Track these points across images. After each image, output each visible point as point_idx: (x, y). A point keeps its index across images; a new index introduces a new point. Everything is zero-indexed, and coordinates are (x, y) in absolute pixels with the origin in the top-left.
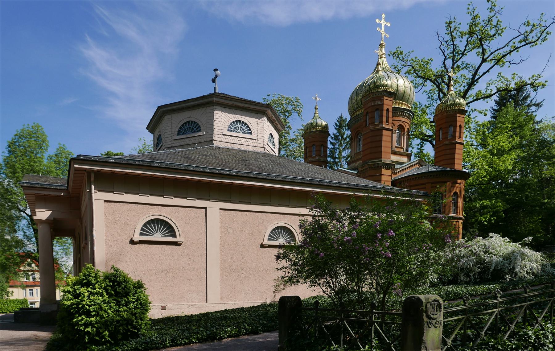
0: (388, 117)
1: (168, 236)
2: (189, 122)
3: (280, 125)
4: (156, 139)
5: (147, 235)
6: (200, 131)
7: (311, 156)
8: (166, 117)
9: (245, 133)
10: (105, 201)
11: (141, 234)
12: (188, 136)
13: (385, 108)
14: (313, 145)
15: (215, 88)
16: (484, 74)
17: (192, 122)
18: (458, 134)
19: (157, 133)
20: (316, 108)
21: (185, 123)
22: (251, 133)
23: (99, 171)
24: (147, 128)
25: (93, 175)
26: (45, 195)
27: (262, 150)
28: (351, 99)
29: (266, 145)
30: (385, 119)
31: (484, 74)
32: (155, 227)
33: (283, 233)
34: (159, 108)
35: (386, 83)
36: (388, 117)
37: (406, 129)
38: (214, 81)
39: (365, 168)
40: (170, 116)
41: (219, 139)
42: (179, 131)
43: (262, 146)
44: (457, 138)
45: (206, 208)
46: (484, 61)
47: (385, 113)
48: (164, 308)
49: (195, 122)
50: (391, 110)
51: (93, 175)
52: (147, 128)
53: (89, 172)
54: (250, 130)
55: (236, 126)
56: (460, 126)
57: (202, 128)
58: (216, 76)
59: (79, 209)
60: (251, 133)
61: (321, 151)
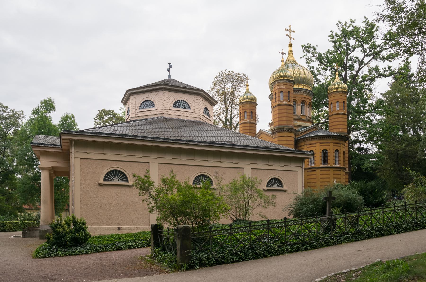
2: (147, 100)
5: (109, 180)
7: (244, 119)
9: (185, 108)
10: (81, 158)
11: (105, 180)
14: (245, 111)
17: (149, 100)
21: (145, 101)
22: (190, 108)
23: (78, 140)
24: (122, 102)
25: (73, 143)
27: (197, 120)
32: (114, 175)
34: (128, 91)
35: (286, 74)
38: (168, 70)
43: (198, 117)
45: (149, 163)
48: (119, 229)
49: (151, 101)
51: (73, 143)
52: (122, 102)
53: (71, 141)
54: (189, 106)
55: (178, 104)
57: (155, 105)
59: (69, 160)
60: (190, 108)
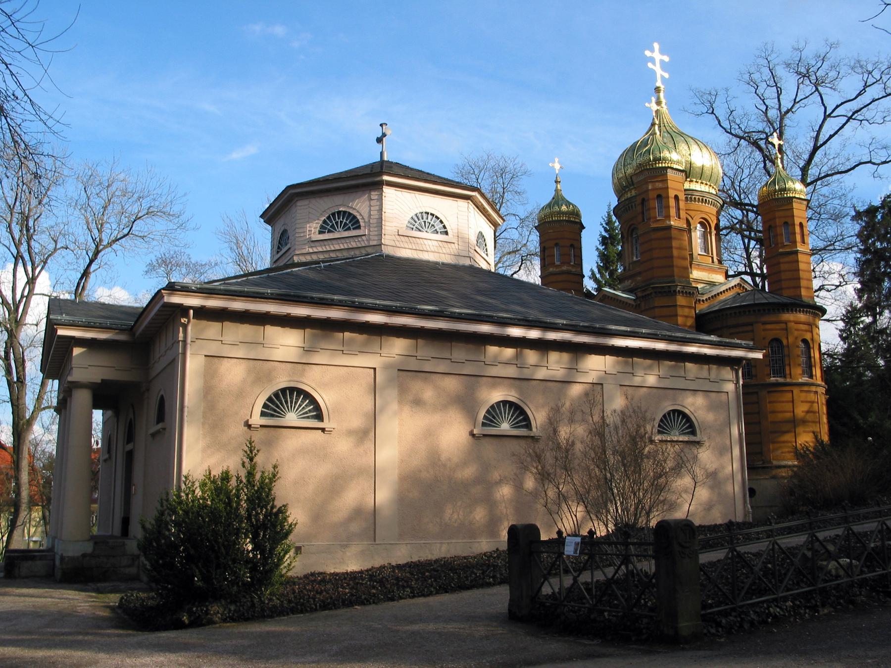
0: (678, 209)
1: (308, 417)
3: (492, 206)
4: (278, 236)
6: (359, 227)
8: (299, 203)
12: (336, 235)
13: (672, 194)
15: (382, 154)
16: (831, 137)
18: (798, 238)
19: (280, 228)
20: (556, 182)
22: (446, 233)
24: (261, 216)
26: (93, 339)
28: (616, 170)
29: (472, 251)
30: (673, 212)
31: (831, 137)
33: (302, 208)
36: (678, 209)
37: (713, 226)
38: (379, 140)
39: (648, 292)
40: (306, 202)
41: (392, 243)
42: (322, 227)
44: (798, 244)
46: (826, 116)
47: (672, 202)
50: (682, 197)
56: (801, 225)
57: (362, 224)
58: (384, 135)
61: (570, 255)
